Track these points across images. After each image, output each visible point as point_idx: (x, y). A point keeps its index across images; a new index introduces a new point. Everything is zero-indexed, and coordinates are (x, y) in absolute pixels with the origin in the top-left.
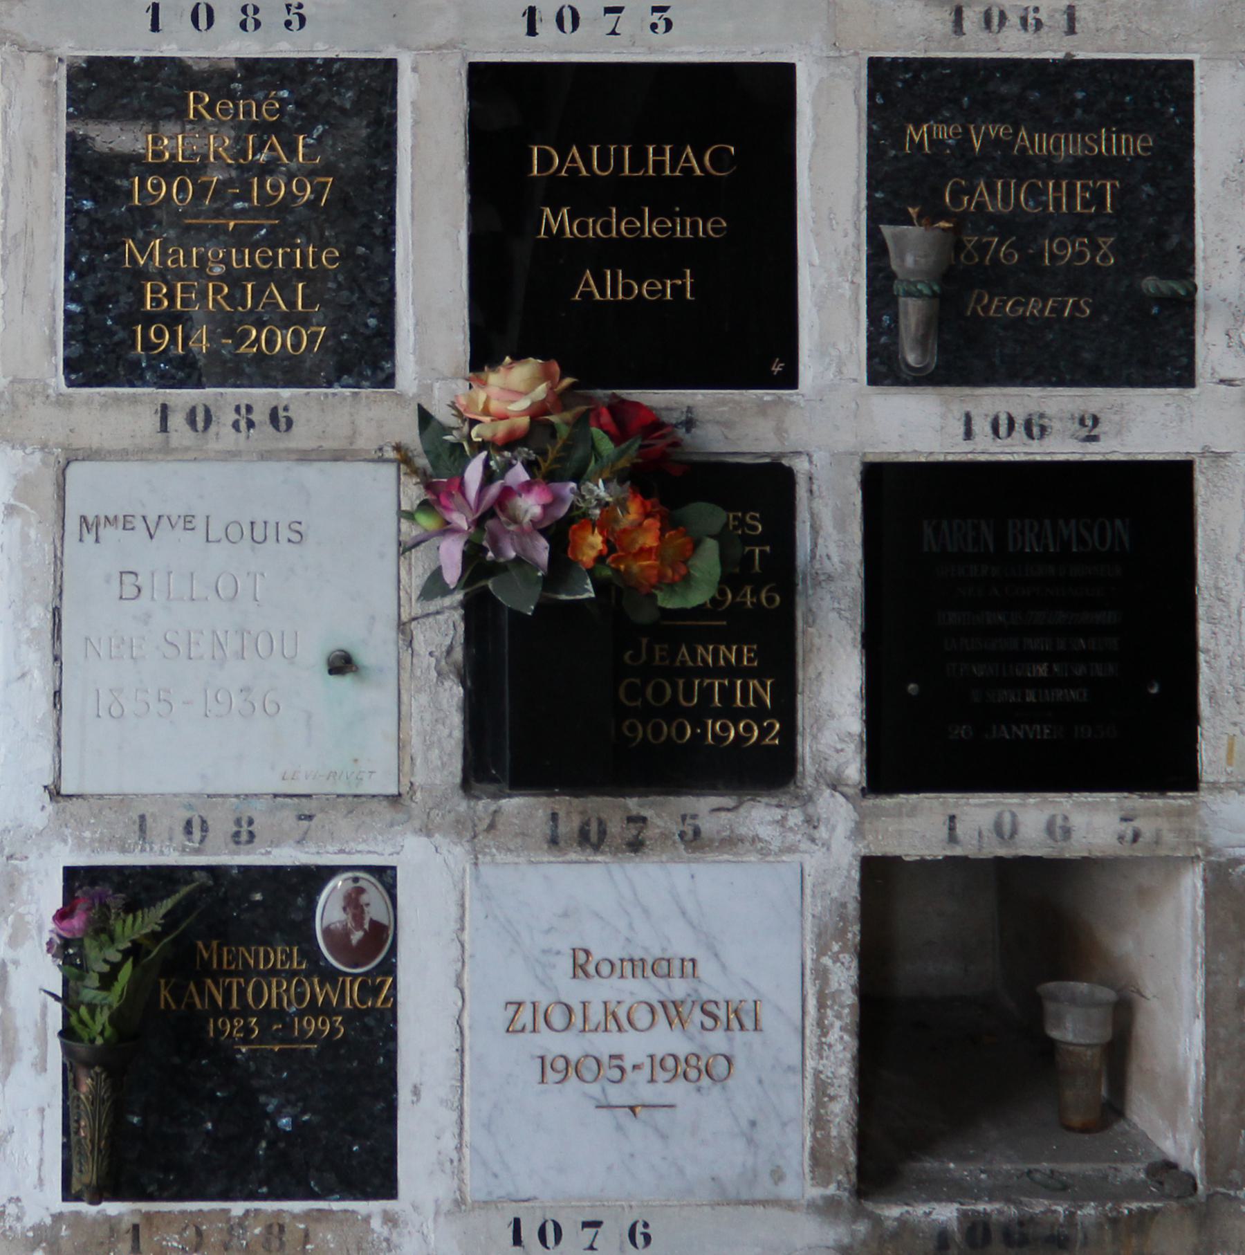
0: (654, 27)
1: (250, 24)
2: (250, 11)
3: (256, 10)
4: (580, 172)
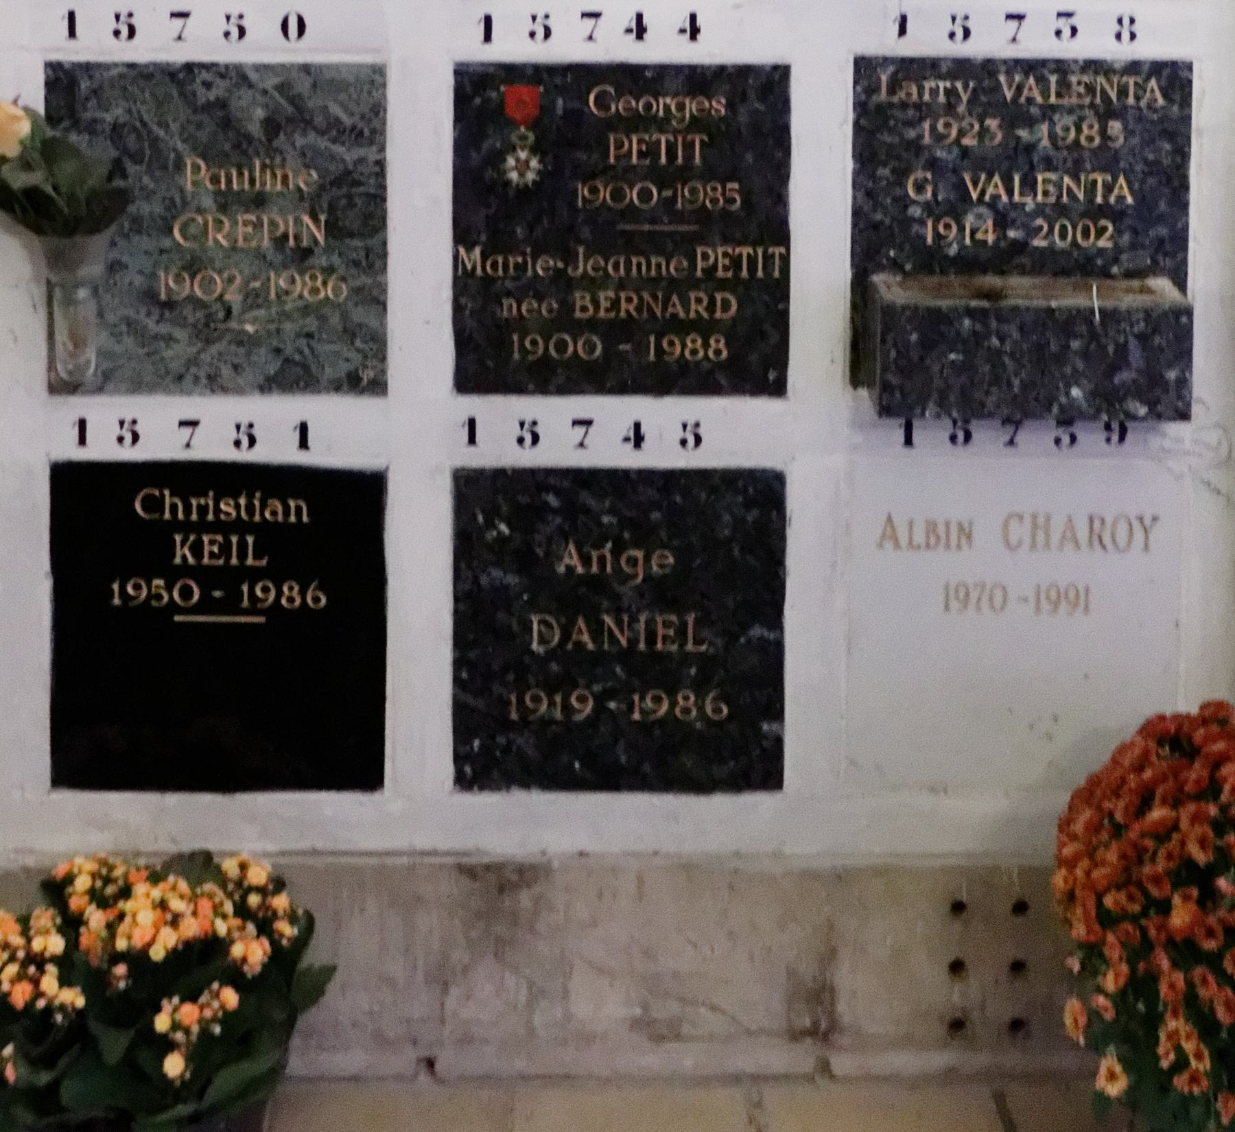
0: (1058, 33)
1: (1126, 36)
2: (1126, 22)
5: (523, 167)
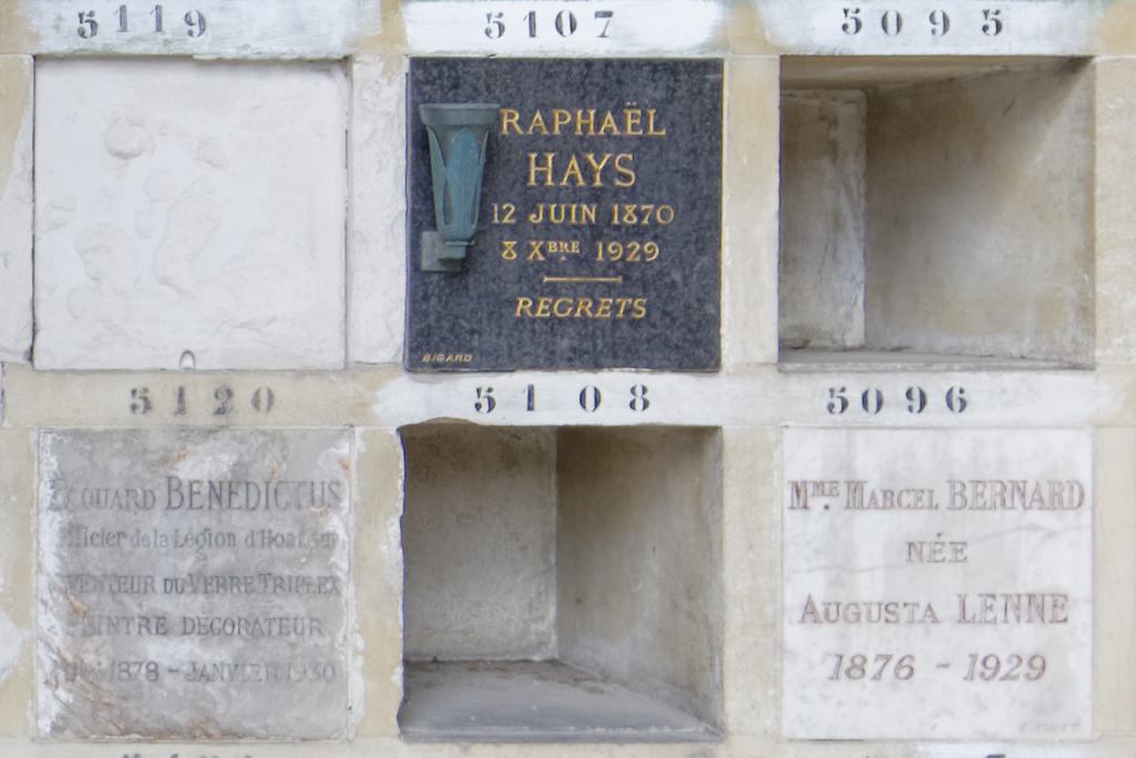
1: (639, 404)
2: (639, 391)
3: (644, 390)
4: (577, 181)
5: (509, 254)
